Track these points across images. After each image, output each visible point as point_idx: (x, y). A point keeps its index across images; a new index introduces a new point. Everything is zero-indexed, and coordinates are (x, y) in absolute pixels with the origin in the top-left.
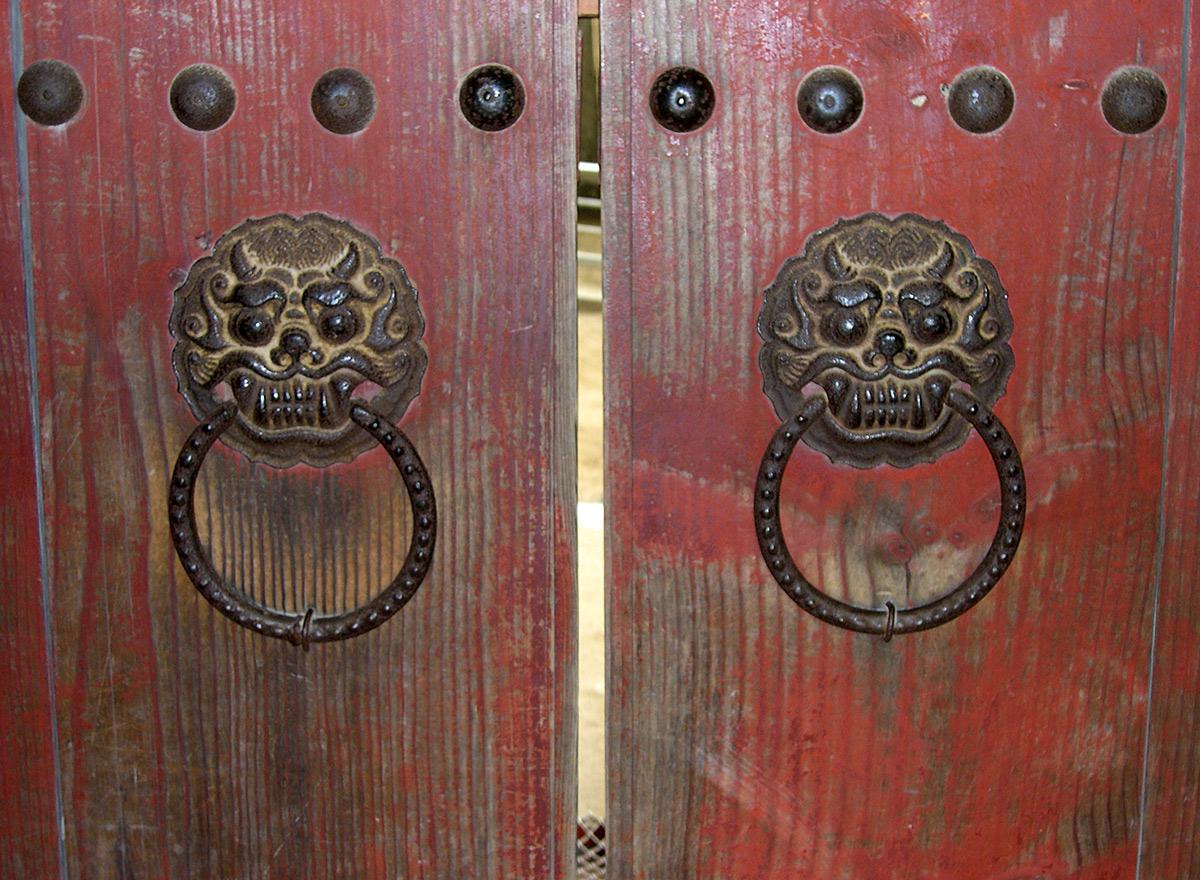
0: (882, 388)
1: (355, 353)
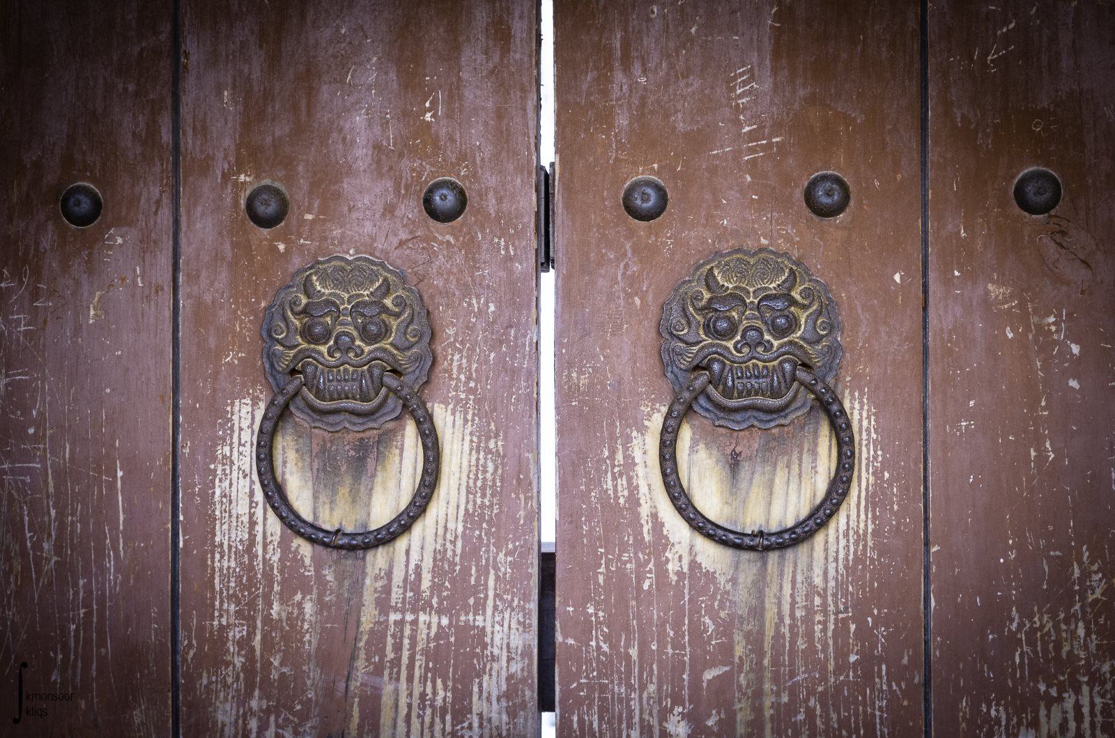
0: (747, 367)
1: (385, 350)
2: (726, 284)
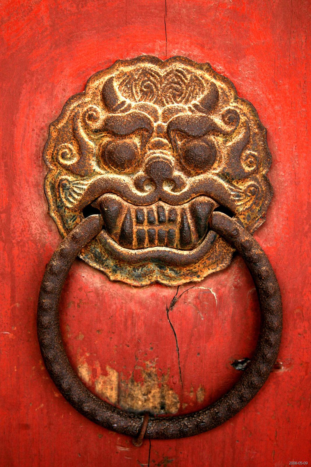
2: (128, 101)
